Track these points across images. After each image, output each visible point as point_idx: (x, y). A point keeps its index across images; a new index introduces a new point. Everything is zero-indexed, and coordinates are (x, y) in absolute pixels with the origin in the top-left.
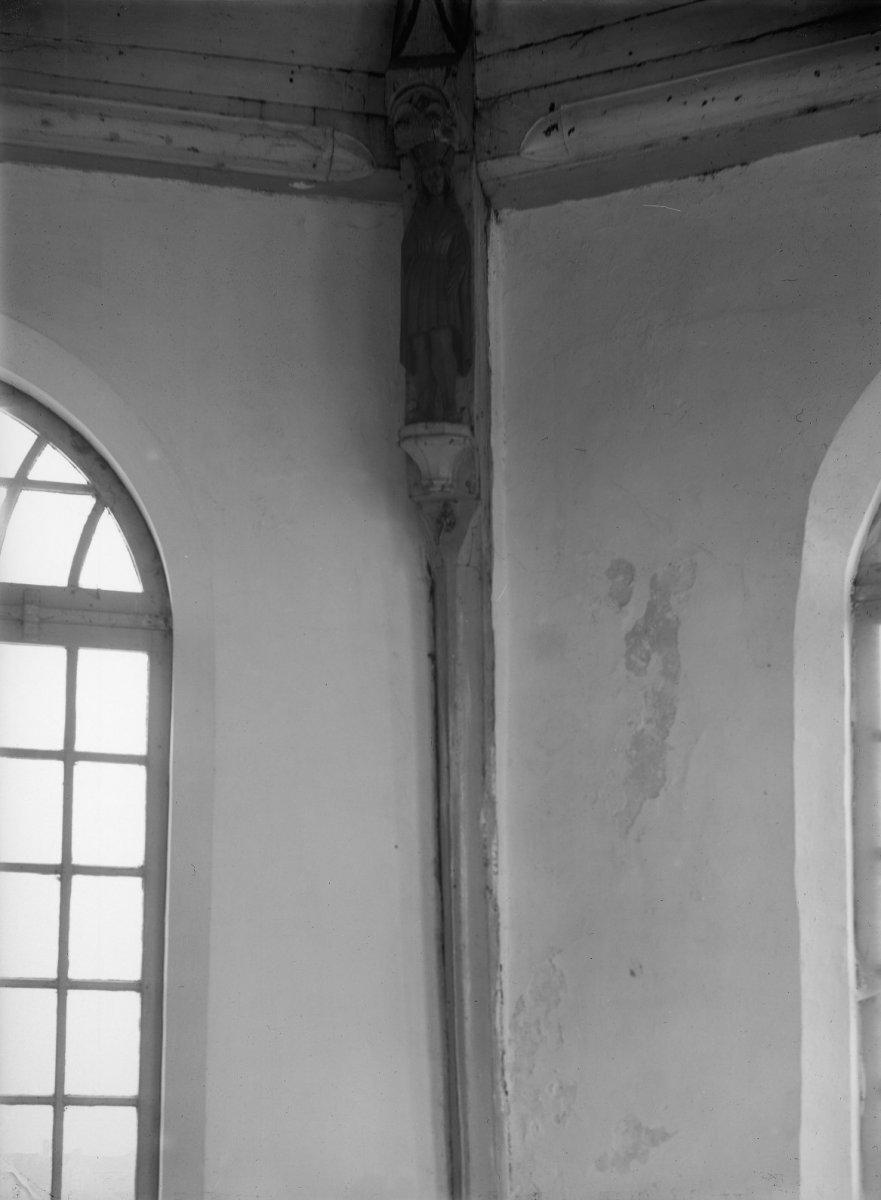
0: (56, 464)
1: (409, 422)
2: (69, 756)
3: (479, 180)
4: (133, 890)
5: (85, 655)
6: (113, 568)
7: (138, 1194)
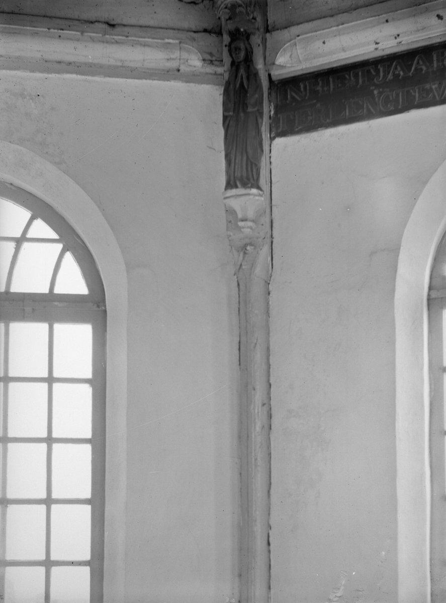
0: (41, 229)
1: (230, 185)
2: (50, 440)
3: (271, 274)
4: (87, 391)
5: (57, 326)
6: (73, 281)
7: (91, 601)
